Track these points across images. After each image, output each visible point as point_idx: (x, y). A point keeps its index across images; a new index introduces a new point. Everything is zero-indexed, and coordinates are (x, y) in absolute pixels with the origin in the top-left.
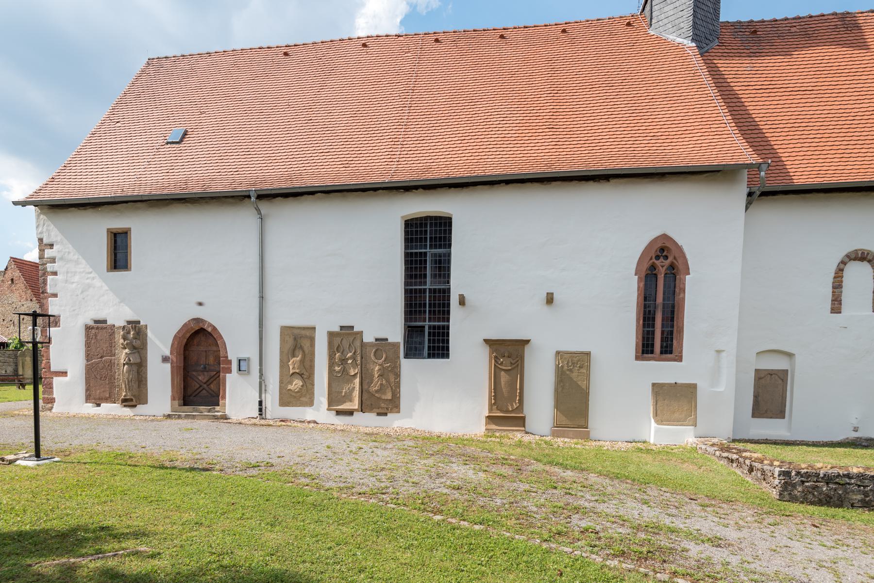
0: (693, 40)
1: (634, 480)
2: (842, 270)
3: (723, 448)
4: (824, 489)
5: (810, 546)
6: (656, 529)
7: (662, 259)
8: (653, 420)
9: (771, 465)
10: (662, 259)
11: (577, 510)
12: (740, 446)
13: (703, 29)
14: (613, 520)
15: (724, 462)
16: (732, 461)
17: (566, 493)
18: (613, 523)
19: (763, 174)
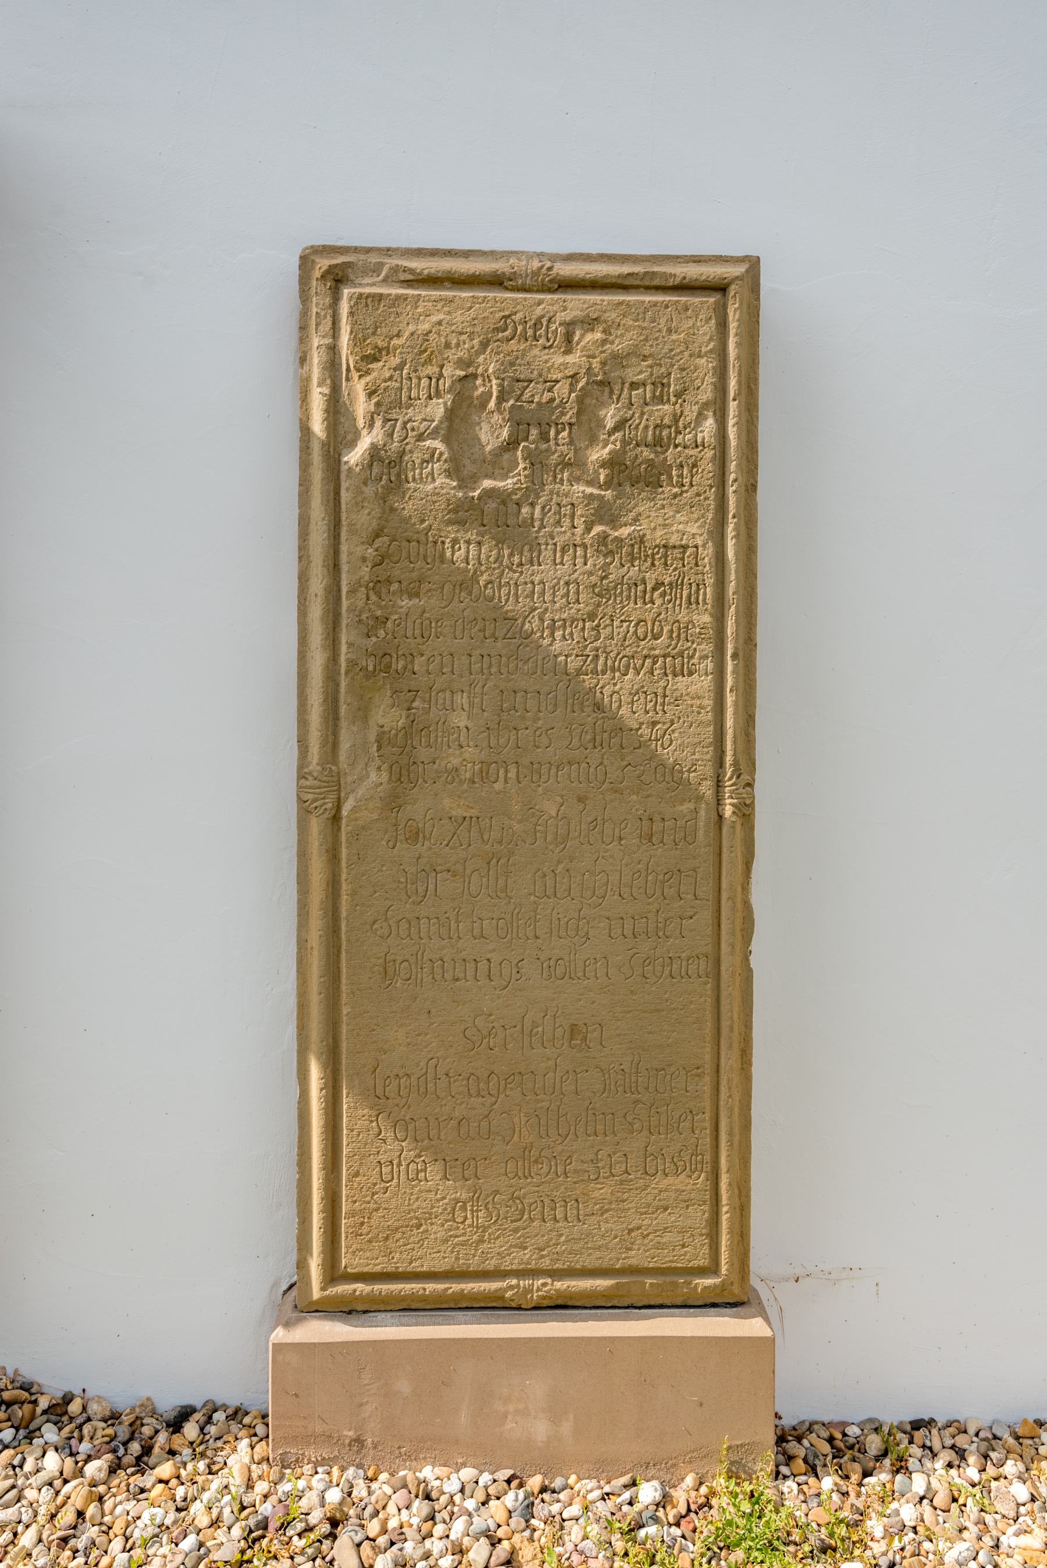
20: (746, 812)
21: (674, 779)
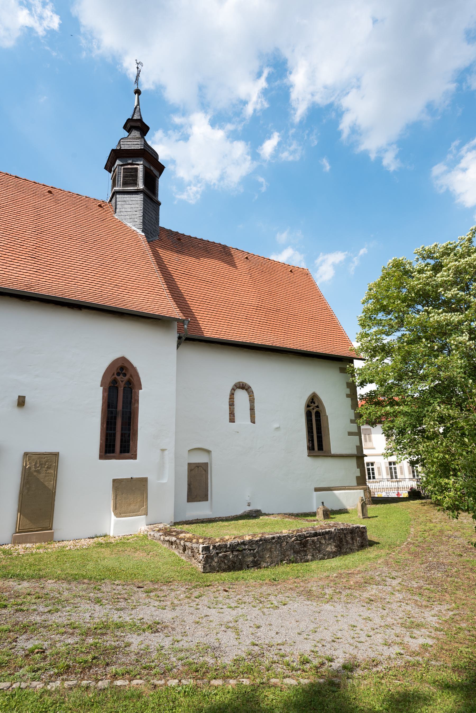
0: (143, 231)
1: (90, 579)
2: (233, 394)
3: (167, 533)
4: (231, 556)
5: (221, 611)
6: (103, 629)
7: (121, 376)
8: (113, 513)
9: (197, 543)
10: (121, 376)
11: (25, 629)
12: (178, 528)
13: (149, 227)
14: (63, 630)
15: (166, 545)
16: (172, 543)
17: (17, 611)
18: (63, 634)
19: (186, 326)
20: (55, 492)
21: (50, 490)
